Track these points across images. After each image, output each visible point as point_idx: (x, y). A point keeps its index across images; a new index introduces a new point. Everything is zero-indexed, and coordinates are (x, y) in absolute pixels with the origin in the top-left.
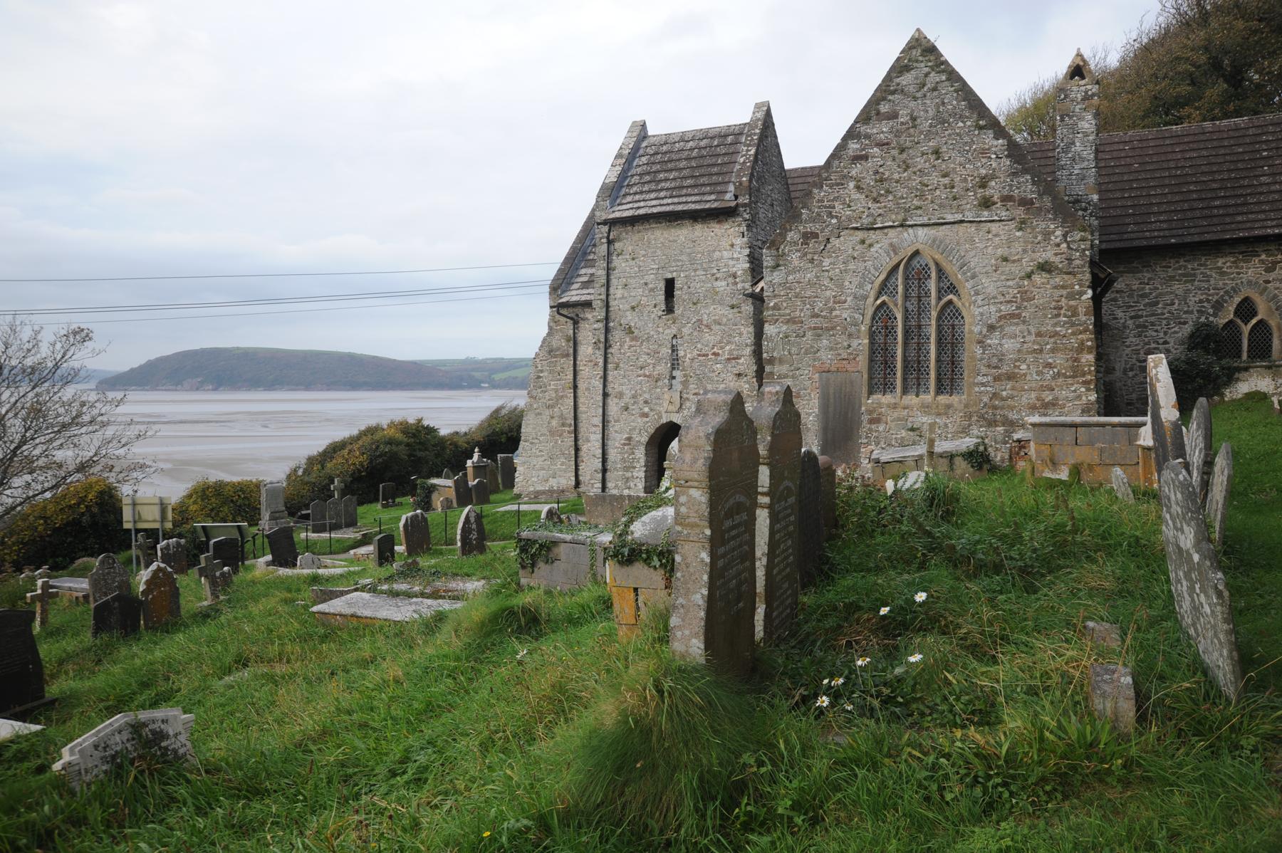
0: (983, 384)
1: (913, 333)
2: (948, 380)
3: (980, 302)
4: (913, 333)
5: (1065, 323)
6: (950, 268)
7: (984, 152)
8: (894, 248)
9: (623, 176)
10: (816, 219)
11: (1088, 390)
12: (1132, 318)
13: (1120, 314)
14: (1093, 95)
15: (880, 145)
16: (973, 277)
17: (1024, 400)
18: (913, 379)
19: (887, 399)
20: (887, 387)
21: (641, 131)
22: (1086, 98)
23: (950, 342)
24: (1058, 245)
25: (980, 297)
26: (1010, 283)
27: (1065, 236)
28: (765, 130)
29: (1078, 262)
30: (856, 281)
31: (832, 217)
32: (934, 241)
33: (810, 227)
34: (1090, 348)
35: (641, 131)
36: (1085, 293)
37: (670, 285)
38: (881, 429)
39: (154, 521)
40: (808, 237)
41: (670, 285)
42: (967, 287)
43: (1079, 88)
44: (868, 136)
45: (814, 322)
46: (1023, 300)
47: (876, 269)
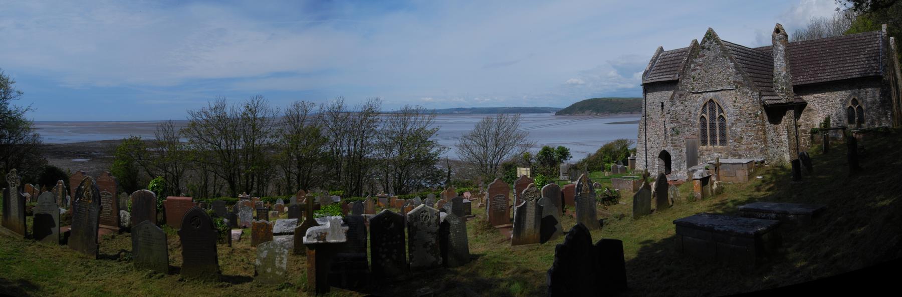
1: (713, 125)
2: (723, 141)
4: (713, 125)
9: (651, 68)
19: (705, 147)
20: (704, 143)
23: (723, 129)
28: (696, 42)
40: (681, 95)
42: (725, 110)
43: (778, 36)
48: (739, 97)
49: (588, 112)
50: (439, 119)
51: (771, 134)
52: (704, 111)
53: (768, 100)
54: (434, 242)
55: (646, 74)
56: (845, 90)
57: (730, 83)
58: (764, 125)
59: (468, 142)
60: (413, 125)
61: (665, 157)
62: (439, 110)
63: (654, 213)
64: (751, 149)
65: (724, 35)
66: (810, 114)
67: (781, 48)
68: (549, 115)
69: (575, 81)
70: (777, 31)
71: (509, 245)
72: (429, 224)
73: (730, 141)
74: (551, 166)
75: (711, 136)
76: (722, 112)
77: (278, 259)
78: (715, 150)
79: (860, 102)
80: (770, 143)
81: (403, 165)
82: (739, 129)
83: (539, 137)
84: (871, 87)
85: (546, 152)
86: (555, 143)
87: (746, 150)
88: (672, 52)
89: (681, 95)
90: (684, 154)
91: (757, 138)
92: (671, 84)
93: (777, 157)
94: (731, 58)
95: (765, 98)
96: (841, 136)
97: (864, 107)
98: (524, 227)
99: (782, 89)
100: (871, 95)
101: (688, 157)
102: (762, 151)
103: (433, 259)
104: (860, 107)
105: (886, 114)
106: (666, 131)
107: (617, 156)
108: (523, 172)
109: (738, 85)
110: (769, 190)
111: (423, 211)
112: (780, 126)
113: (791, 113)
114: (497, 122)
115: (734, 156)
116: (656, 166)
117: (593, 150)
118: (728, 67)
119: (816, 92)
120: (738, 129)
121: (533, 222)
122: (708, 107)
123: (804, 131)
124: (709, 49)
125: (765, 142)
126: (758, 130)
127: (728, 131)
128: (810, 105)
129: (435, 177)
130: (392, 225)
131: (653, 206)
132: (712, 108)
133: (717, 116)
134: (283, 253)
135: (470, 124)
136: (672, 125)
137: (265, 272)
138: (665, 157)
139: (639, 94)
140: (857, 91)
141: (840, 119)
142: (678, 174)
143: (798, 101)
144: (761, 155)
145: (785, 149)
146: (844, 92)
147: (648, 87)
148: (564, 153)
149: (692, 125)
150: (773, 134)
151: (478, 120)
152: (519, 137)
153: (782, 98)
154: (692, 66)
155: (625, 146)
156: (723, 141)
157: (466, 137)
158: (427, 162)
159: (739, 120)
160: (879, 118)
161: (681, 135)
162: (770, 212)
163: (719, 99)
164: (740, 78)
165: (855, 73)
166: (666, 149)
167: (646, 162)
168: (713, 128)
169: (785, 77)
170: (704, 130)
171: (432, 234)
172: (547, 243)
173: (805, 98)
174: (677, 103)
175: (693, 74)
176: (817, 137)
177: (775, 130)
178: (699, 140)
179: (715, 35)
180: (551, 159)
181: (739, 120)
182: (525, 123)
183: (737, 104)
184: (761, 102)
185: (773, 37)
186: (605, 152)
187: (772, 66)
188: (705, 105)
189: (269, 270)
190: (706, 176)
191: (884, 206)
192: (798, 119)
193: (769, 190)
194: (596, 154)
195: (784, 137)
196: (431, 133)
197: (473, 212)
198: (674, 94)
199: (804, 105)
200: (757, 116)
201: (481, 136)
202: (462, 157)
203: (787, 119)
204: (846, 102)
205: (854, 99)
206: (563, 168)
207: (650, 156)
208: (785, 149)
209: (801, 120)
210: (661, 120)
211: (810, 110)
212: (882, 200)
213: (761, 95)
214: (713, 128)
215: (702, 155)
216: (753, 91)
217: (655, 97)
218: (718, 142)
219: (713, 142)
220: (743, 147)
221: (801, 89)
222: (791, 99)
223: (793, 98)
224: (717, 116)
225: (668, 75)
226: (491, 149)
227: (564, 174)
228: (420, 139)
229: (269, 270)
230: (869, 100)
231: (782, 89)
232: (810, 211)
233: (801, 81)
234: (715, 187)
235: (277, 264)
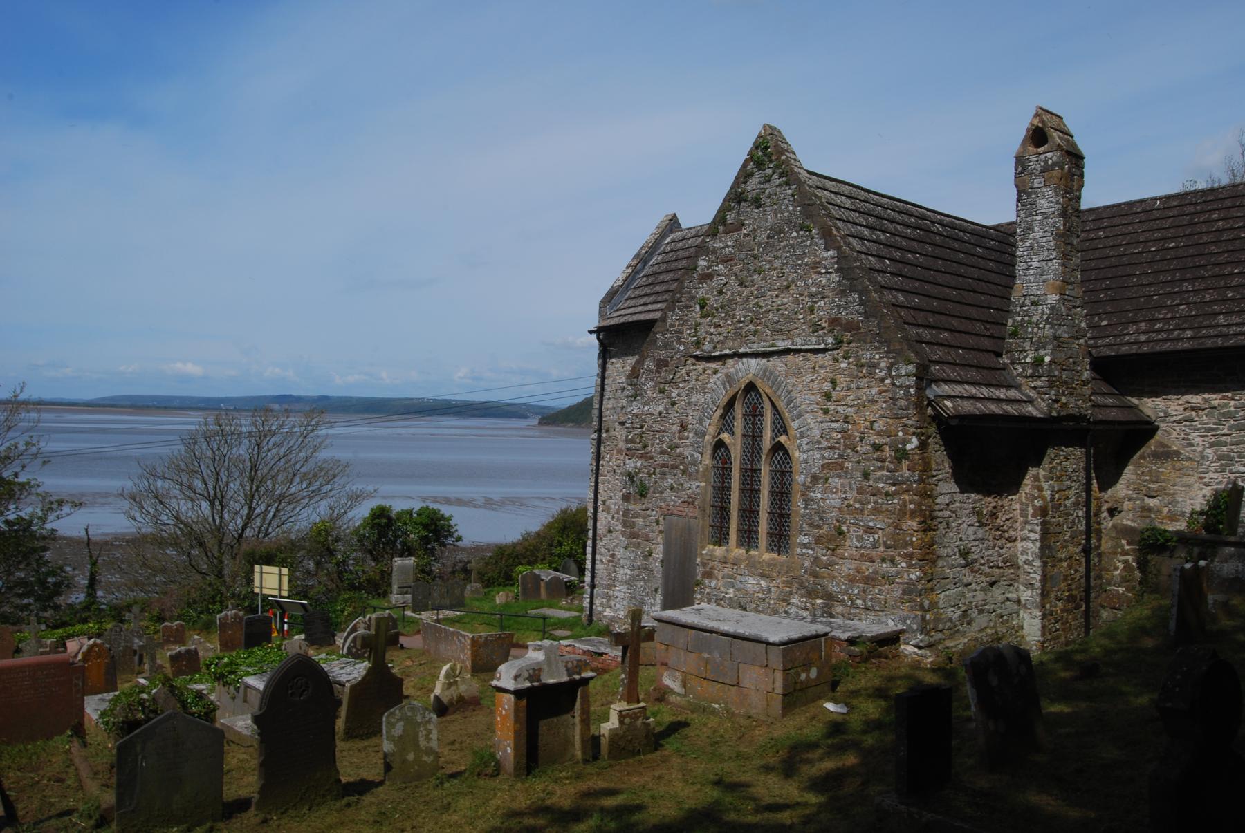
0: (805, 546)
1: (750, 475)
2: (780, 540)
3: (805, 447)
4: (750, 475)
5: (889, 478)
6: (781, 405)
8: (729, 379)
10: (666, 346)
11: (910, 566)
12: (1212, 445)
13: (1196, 438)
14: (1054, 164)
15: (727, 260)
16: (799, 416)
17: (845, 571)
19: (719, 551)
20: (721, 538)
22: (1046, 169)
23: (781, 494)
24: (882, 380)
25: (805, 441)
26: (834, 425)
27: (889, 369)
29: (903, 403)
30: (697, 414)
31: (680, 343)
32: (765, 372)
33: (664, 355)
34: (913, 513)
35: (673, 223)
36: (909, 442)
38: (713, 585)
39: (261, 588)
40: (661, 364)
43: (1036, 159)
44: (714, 251)
45: (664, 459)
46: (846, 446)
47: (714, 403)
48: (843, 381)
53: (955, 397)
55: (611, 297)
57: (816, 327)
58: (927, 495)
64: (869, 580)
65: (816, 154)
66: (1165, 469)
68: (521, 423)
70: (1038, 136)
76: (785, 431)
77: (422, 733)
78: (752, 565)
80: (950, 565)
82: (834, 501)
86: (404, 498)
87: (852, 580)
89: (661, 364)
91: (897, 541)
94: (826, 234)
99: (1038, 362)
101: (666, 577)
109: (844, 334)
113: (1069, 460)
118: (815, 266)
119: (1196, 388)
122: (739, 410)
124: (757, 202)
126: (903, 513)
127: (798, 504)
128: (1170, 435)
133: (767, 443)
134: (429, 722)
135: (190, 423)
136: (631, 465)
137: (404, 761)
143: (1113, 414)
144: (904, 610)
149: (680, 465)
152: (329, 473)
153: (1035, 401)
154: (702, 263)
159: (836, 466)
161: (652, 499)
163: (775, 384)
164: (852, 310)
169: (1055, 317)
170: (722, 491)
173: (1151, 406)
174: (649, 388)
176: (1168, 566)
178: (702, 523)
181: (836, 466)
182: (340, 441)
183: (839, 406)
184: (921, 403)
185: (1020, 161)
188: (730, 404)
189: (411, 757)
192: (1108, 481)
195: (1028, 547)
198: (640, 363)
199: (1141, 432)
200: (901, 455)
206: (403, 569)
208: (1026, 595)
209: (1121, 489)
211: (1166, 455)
213: (924, 377)
215: (709, 575)
216: (896, 357)
218: (733, 536)
219: (748, 537)
222: (1075, 405)
223: (1088, 400)
224: (767, 443)
226: (237, 504)
227: (403, 589)
229: (411, 757)
231: (1038, 362)
233: (1136, 339)
235: (422, 743)
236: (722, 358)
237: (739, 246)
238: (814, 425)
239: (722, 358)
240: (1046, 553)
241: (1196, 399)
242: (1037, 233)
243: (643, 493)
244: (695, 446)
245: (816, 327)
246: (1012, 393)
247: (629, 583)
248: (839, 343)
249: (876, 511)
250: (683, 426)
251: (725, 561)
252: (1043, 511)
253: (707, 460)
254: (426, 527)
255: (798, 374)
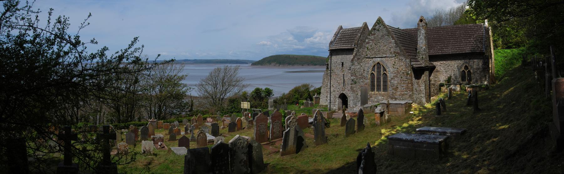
1: (379, 79)
2: (385, 89)
4: (379, 79)
6: (385, 66)
7: (391, 42)
9: (335, 39)
10: (359, 55)
15: (372, 40)
18: (379, 89)
19: (373, 93)
20: (373, 90)
21: (341, 28)
23: (385, 82)
28: (366, 25)
33: (359, 57)
35: (341, 28)
37: (343, 63)
40: (358, 59)
41: (343, 63)
42: (387, 70)
43: (421, 24)
48: (397, 62)
49: (273, 64)
50: (187, 67)
51: (416, 86)
52: (373, 70)
53: (415, 65)
54: (245, 159)
55: (331, 43)
56: (461, 60)
57: (391, 53)
59: (203, 83)
60: (170, 71)
61: (344, 98)
62: (189, 60)
63: (356, 133)
65: (387, 21)
66: (438, 74)
67: (423, 31)
68: (247, 65)
69: (265, 42)
70: (421, 21)
71: (278, 156)
72: (242, 147)
73: (390, 89)
74: (260, 100)
75: (377, 85)
76: (385, 70)
78: (380, 95)
79: (469, 68)
81: (162, 100)
82: (396, 82)
83: (253, 81)
84: (475, 59)
85: (258, 92)
87: (400, 95)
88: (349, 30)
89: (358, 59)
90: (359, 96)
91: (407, 88)
92: (349, 51)
93: (418, 100)
94: (392, 37)
95: (413, 63)
96: (459, 89)
97: (471, 71)
98: (288, 144)
99: (423, 58)
100: (476, 64)
102: (410, 96)
103: (245, 170)
104: (469, 71)
105: (485, 76)
106: (344, 81)
107: (303, 95)
108: (245, 105)
109: (396, 54)
110: (419, 120)
111: (239, 139)
112: (420, 81)
113: (427, 73)
114: (223, 71)
115: (392, 98)
116: (337, 103)
117: (287, 91)
120: (395, 82)
121: (293, 141)
122: (376, 67)
123: (434, 85)
124: (378, 30)
125: (412, 90)
126: (408, 83)
127: (389, 83)
128: (438, 68)
129: (182, 107)
130: (222, 151)
131: (356, 129)
132: (379, 68)
133: (382, 73)
135: (206, 71)
136: (352, 78)
138: (344, 98)
139: (327, 54)
140: (467, 61)
141: (456, 77)
142: (355, 109)
143: (431, 65)
144: (409, 99)
145: (423, 95)
146: (459, 61)
147: (333, 52)
148: (269, 92)
149: (365, 78)
150: (416, 86)
151: (212, 68)
153: (422, 63)
154: (367, 40)
155: (308, 89)
156: (385, 89)
157: (203, 80)
158: (179, 96)
160: (481, 78)
161: (357, 84)
162: (435, 132)
163: (383, 62)
164: (398, 50)
165: (468, 50)
166: (344, 92)
167: (328, 100)
168: (379, 81)
170: (373, 82)
171: (244, 154)
172: (300, 153)
173: (435, 63)
175: (367, 46)
177: (418, 83)
178: (369, 88)
179: (383, 22)
180: (260, 97)
182: (244, 72)
183: (395, 66)
185: (418, 24)
186: (295, 93)
187: (416, 43)
188: (374, 66)
190: (382, 111)
191: (504, 129)
193: (419, 120)
194: (289, 94)
195: (423, 88)
196: (181, 78)
197: (220, 132)
201: (213, 79)
202: (200, 94)
203: (424, 77)
204: (461, 68)
205: (466, 66)
206: (271, 102)
207: (332, 96)
208: (423, 95)
209: (431, 77)
210: (341, 74)
211: (438, 71)
212: (500, 126)
213: (411, 61)
214: (379, 81)
215: (371, 97)
216: (406, 58)
217: (337, 59)
220: (398, 93)
221: (433, 58)
222: (428, 64)
224: (382, 73)
225: (348, 43)
227: (271, 107)
228: (173, 82)
230: (475, 67)
231: (423, 58)
232: (460, 131)
233: (433, 52)
234: (387, 118)
236: (372, 58)
237: (375, 38)
238: (391, 70)
239: (372, 58)
240: (425, 89)
241: (442, 62)
242: (421, 36)
243: (355, 83)
244: (367, 74)
245: (391, 53)
246: (419, 63)
247: (353, 100)
248: (396, 56)
249: (404, 83)
250: (364, 70)
251: (374, 94)
252: (425, 82)
253: (369, 76)
254: (267, 92)
255: (388, 61)
